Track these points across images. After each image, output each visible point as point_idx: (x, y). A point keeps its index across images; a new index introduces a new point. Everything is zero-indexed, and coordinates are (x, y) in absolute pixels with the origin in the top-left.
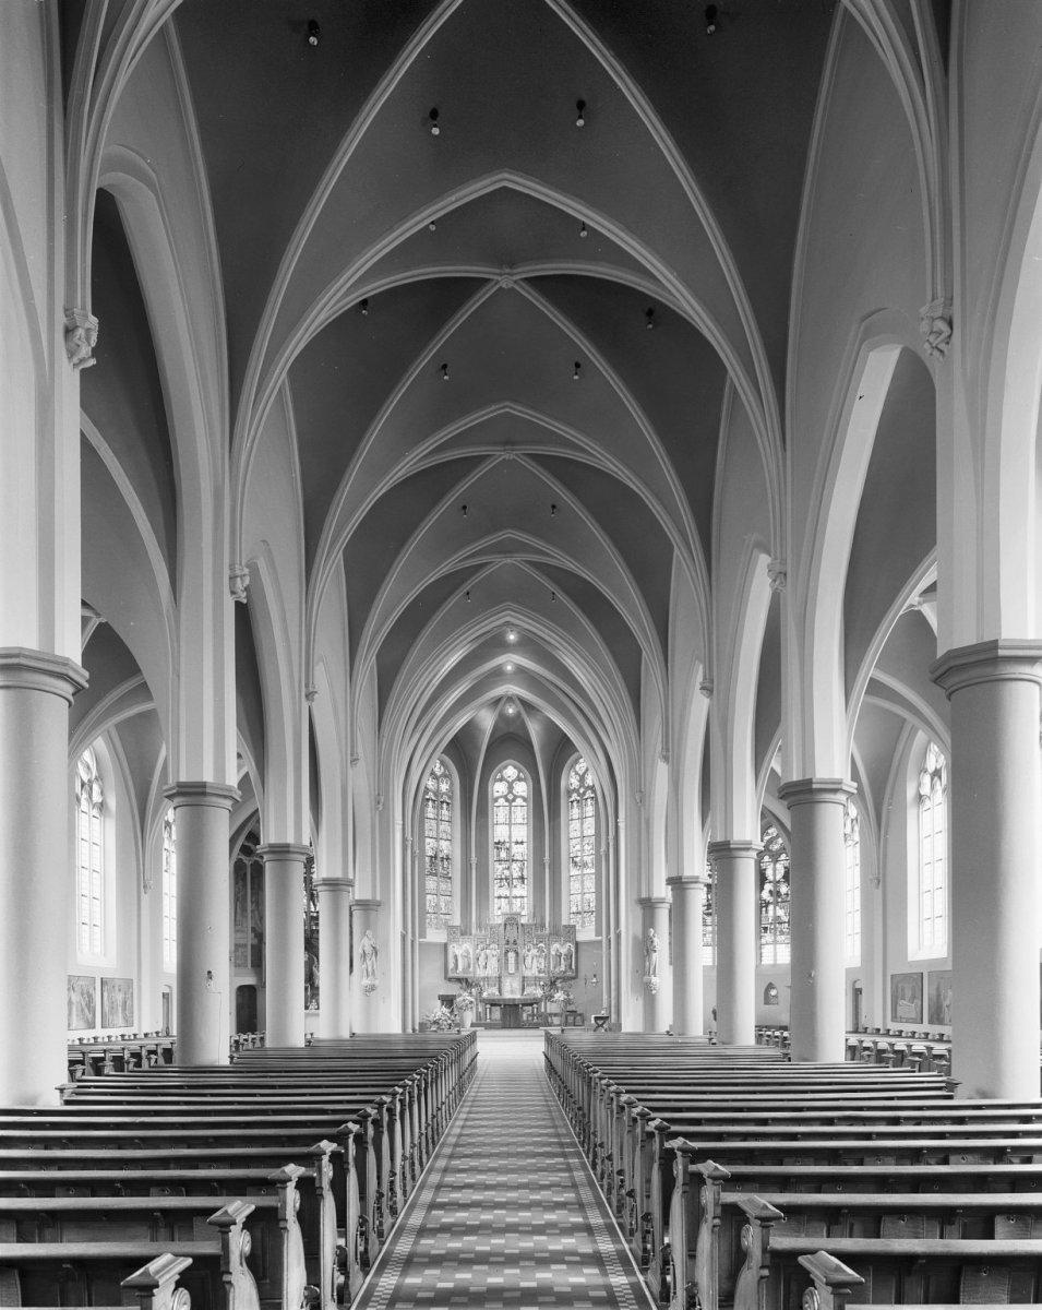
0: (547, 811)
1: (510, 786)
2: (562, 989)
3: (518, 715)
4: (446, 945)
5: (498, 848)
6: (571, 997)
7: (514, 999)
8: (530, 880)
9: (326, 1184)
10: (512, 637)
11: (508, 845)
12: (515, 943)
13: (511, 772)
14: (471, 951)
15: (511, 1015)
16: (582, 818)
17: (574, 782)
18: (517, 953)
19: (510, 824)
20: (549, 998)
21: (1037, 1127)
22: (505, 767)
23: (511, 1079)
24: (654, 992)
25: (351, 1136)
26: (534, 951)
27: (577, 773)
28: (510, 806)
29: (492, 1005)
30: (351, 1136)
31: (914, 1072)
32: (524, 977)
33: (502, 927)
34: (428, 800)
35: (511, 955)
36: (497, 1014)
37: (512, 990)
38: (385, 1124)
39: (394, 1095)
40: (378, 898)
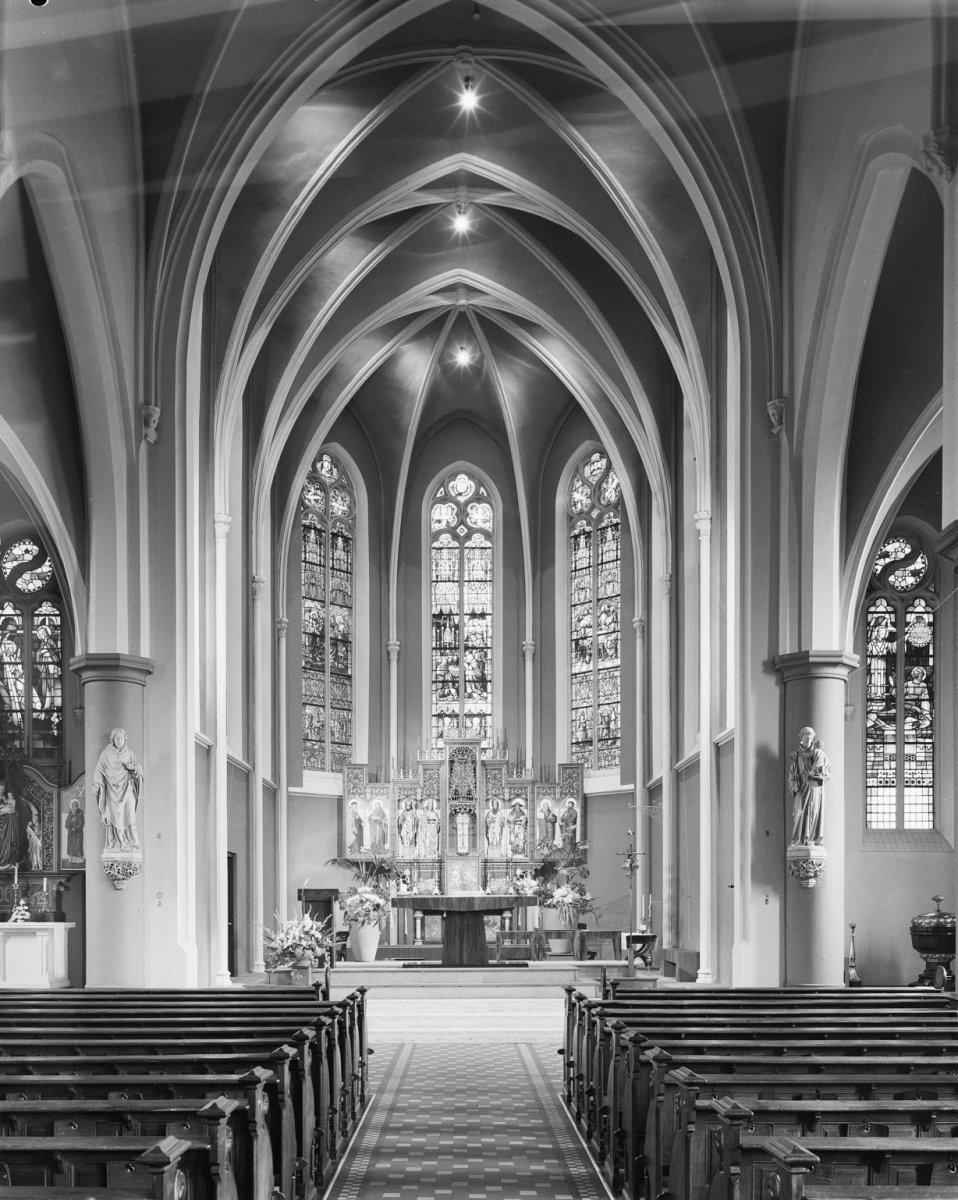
0: (529, 552)
1: (462, 507)
2: (568, 880)
3: (477, 369)
4: (340, 801)
5: (438, 626)
6: (588, 897)
7: (471, 900)
8: (497, 686)
9: (259, 1119)
10: (462, 224)
11: (456, 619)
12: (469, 796)
13: (463, 485)
14: (387, 812)
15: (464, 937)
16: (597, 565)
17: (581, 497)
18: (473, 816)
19: (460, 582)
20: (542, 898)
21: (955, 1020)
22: (453, 476)
23: (465, 1094)
24: (812, 882)
25: (287, 1062)
26: (505, 813)
27: (585, 482)
28: (462, 548)
29: (427, 912)
30: (287, 1062)
31: (939, 992)
32: (486, 861)
33: (447, 766)
34: (307, 528)
35: (463, 820)
36: (435, 928)
37: (463, 884)
38: (324, 1051)
39: (319, 1026)
40: (145, 652)
